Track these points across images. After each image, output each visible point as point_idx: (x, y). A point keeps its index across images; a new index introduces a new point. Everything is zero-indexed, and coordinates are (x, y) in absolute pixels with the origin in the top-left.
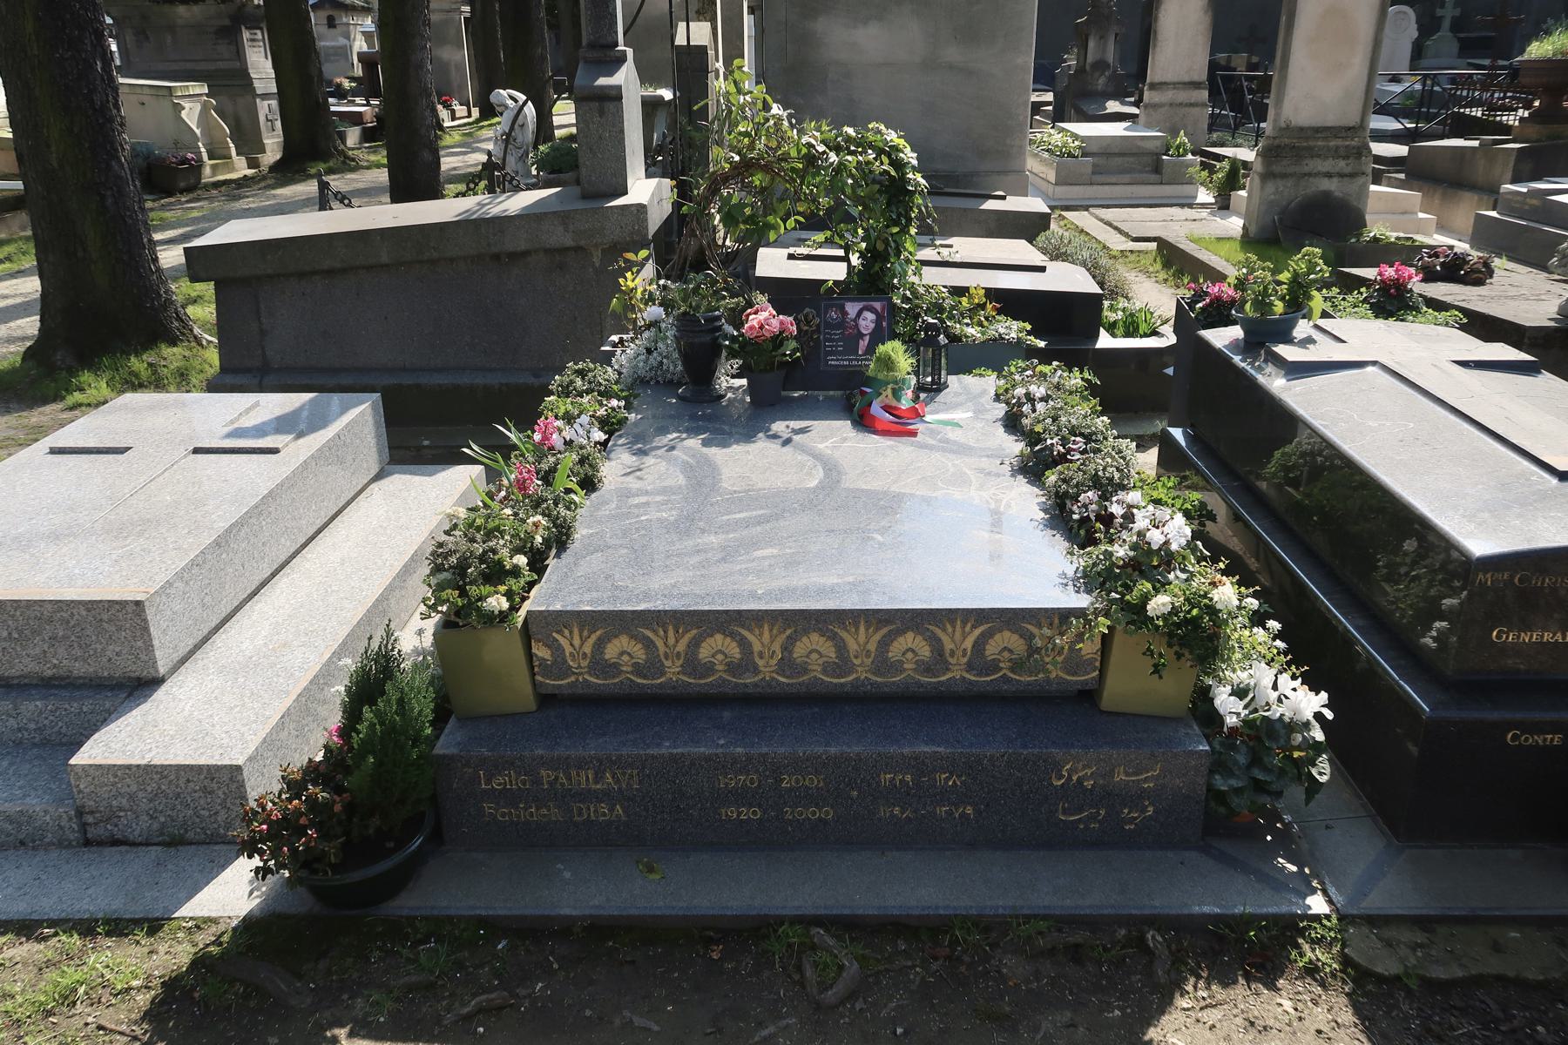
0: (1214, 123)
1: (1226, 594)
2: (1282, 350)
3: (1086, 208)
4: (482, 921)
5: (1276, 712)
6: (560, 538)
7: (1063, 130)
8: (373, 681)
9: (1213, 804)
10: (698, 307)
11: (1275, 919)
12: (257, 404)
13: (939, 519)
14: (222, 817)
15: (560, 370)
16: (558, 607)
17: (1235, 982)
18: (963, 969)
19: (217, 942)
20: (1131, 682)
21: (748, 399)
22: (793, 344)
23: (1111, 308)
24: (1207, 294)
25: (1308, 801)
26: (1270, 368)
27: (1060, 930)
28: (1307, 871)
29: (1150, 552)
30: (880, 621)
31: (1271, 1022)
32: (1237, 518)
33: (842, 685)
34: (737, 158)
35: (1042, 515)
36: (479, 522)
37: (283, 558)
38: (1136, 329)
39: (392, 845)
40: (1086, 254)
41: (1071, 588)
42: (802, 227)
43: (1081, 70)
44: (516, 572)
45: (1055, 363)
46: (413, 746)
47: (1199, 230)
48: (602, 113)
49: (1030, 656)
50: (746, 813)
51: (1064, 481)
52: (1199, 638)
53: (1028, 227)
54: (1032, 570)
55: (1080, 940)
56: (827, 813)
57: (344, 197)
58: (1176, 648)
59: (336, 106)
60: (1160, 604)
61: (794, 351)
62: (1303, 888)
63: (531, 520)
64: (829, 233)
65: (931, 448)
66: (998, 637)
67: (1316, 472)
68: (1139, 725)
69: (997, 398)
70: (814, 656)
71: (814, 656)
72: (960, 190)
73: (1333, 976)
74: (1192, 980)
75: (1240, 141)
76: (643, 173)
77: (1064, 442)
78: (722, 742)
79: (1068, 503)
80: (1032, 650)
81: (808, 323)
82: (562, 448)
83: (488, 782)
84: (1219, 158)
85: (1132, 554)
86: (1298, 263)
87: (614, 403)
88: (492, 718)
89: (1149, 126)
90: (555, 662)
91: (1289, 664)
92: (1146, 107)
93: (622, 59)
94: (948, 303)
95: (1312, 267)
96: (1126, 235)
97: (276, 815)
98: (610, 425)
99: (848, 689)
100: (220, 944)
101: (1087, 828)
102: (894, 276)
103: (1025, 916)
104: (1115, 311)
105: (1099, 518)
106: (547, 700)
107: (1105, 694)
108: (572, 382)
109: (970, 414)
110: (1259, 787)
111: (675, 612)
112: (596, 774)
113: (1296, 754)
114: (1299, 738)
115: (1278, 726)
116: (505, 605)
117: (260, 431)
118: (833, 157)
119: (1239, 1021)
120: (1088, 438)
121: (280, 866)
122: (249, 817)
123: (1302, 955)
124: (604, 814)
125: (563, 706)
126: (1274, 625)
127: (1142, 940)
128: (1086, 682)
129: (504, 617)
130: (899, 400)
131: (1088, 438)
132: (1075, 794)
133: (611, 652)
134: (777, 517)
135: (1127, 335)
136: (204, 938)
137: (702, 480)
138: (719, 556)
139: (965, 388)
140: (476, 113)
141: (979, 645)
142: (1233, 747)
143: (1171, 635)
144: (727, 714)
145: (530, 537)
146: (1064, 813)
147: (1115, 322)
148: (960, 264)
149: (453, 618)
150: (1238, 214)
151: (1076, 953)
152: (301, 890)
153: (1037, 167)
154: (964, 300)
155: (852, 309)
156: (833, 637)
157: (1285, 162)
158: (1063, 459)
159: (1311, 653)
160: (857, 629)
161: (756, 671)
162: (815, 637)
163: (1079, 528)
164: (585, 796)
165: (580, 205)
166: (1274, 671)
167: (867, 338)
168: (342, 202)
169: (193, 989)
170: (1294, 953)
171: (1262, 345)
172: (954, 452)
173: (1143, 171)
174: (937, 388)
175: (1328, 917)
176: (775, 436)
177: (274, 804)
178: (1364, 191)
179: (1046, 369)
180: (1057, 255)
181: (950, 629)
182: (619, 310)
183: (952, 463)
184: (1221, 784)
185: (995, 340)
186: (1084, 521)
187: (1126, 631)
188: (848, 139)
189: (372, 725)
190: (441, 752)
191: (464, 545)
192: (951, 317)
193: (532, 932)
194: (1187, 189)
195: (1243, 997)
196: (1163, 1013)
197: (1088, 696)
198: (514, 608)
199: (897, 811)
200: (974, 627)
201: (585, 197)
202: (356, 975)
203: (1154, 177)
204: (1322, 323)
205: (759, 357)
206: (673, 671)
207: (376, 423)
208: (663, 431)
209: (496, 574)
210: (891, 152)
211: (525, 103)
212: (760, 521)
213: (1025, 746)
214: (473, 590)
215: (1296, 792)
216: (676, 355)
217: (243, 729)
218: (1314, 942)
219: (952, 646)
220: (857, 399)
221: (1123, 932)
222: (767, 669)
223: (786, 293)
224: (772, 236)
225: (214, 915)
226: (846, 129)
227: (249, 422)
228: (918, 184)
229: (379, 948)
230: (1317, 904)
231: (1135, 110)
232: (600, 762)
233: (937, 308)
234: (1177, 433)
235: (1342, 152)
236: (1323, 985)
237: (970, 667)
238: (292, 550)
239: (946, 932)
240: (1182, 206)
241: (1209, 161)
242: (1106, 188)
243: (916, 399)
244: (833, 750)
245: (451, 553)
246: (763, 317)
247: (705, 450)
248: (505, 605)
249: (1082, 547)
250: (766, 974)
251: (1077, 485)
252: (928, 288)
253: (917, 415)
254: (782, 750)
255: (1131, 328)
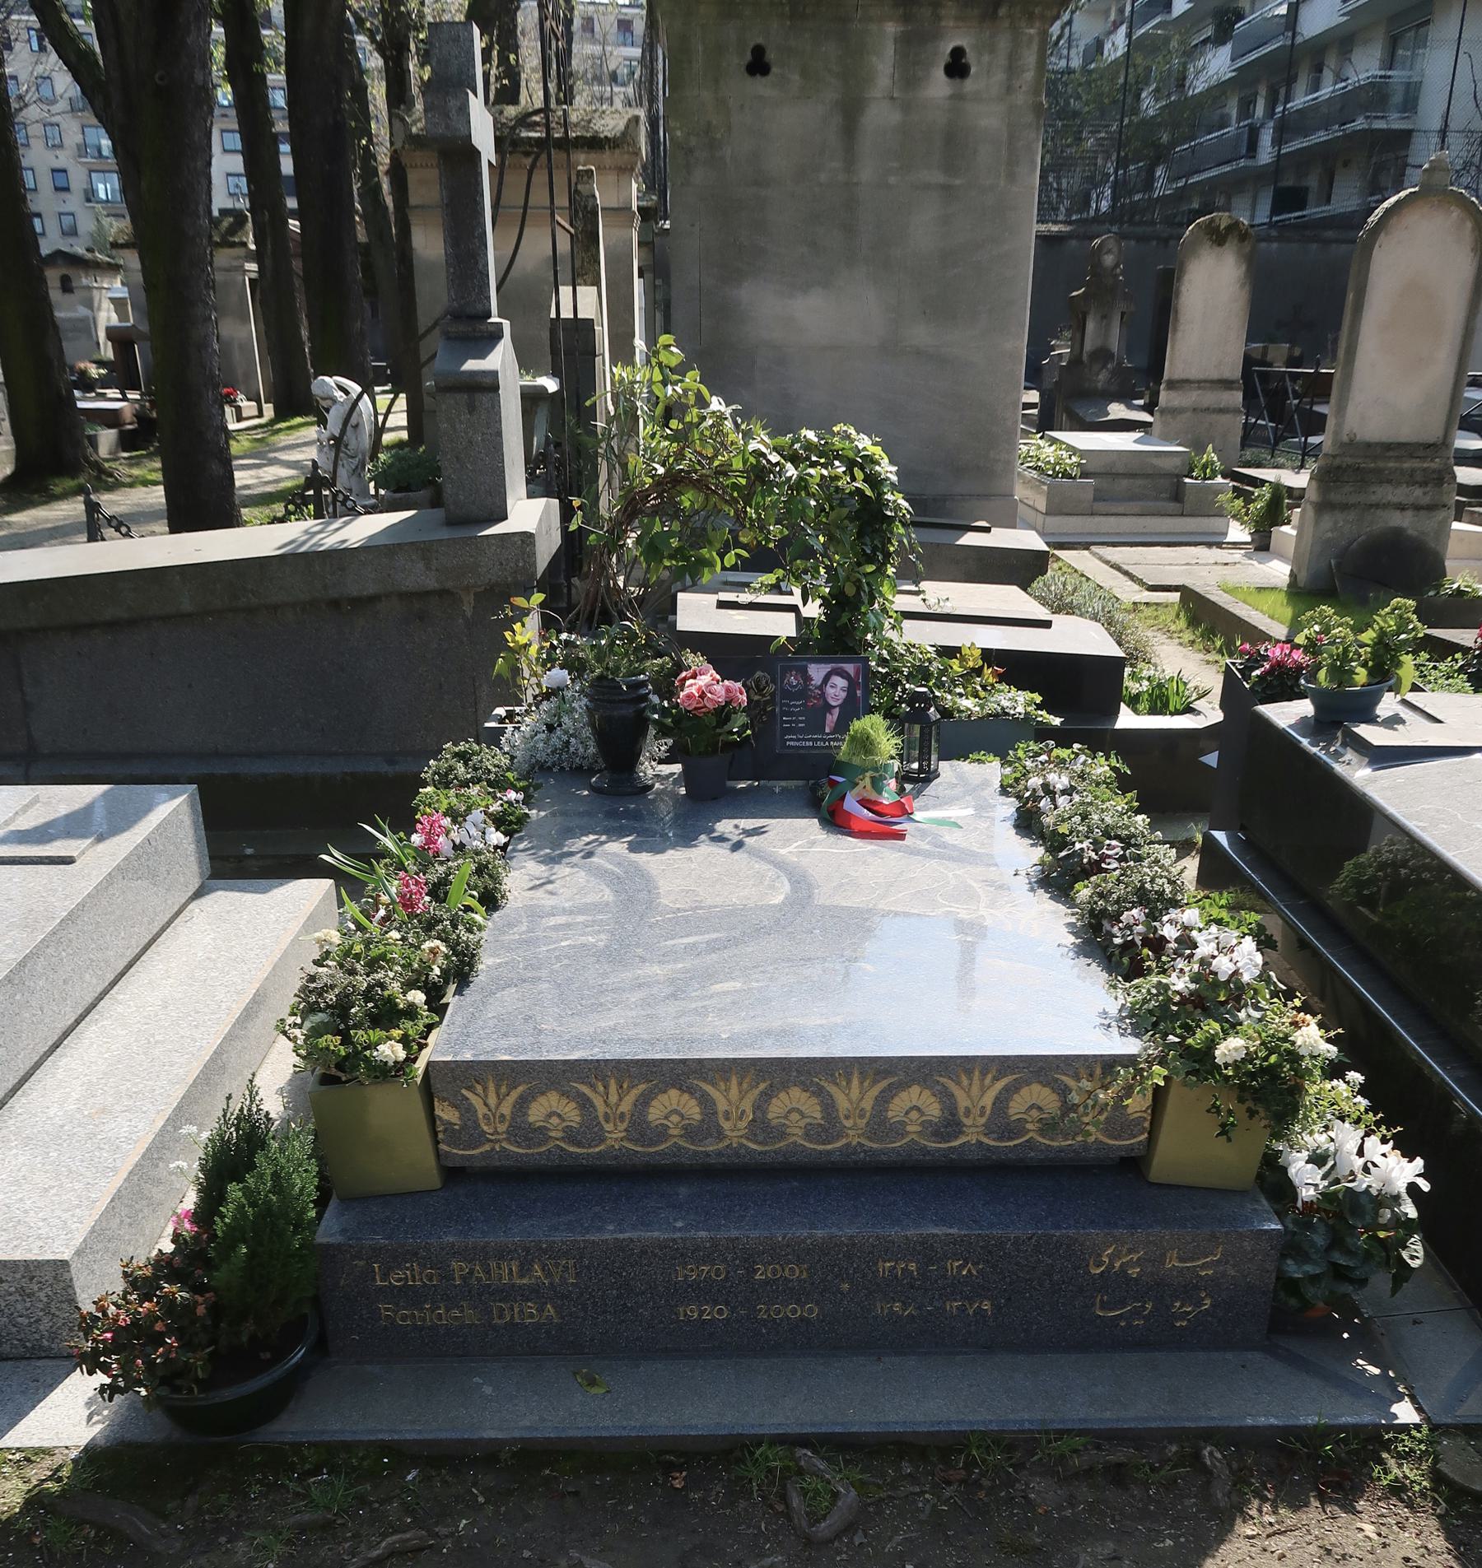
0: (1249, 436)
1: (1311, 1037)
2: (1363, 730)
3: (1086, 546)
4: (386, 1448)
5: (1363, 1183)
6: (462, 970)
7: (1054, 441)
8: (235, 1155)
9: (1282, 1294)
10: (618, 668)
11: (1355, 1430)
12: (36, 800)
13: (938, 947)
14: (45, 1325)
15: (436, 753)
16: (468, 1056)
17: (1307, 1504)
18: (982, 1495)
19: (55, 1476)
20: (1189, 1146)
21: (683, 791)
22: (742, 719)
23: (1133, 675)
24: (1265, 658)
25: (1394, 1291)
26: (1349, 755)
27: (1098, 1447)
28: (1391, 1374)
29: (1216, 985)
30: (878, 1073)
31: (1350, 1550)
32: (1303, 944)
33: (828, 1152)
34: (661, 470)
35: (1072, 939)
36: (358, 949)
37: (89, 1000)
38: (1166, 705)
39: (268, 1355)
40: (1097, 605)
41: (1115, 1031)
42: (747, 566)
43: (1076, 361)
44: (411, 1012)
45: (1076, 746)
46: (295, 1233)
47: (1234, 576)
48: (472, 408)
49: (1064, 1115)
50: (709, 1312)
51: (1101, 895)
52: (1274, 1091)
53: (1021, 569)
54: (1073, 1013)
55: (1123, 1459)
56: (811, 1310)
57: (121, 524)
58: (1250, 1104)
59: (86, 403)
60: (1230, 1049)
61: (744, 727)
62: (1388, 1394)
63: (427, 945)
64: (780, 572)
65: (928, 855)
66: (1024, 1091)
67: (1398, 889)
68: (1198, 1199)
69: (1004, 791)
70: (795, 1116)
71: (795, 1116)
72: (934, 516)
73: (1423, 1495)
74: (1256, 1503)
75: (1281, 460)
76: (522, 490)
77: (1097, 845)
78: (679, 1224)
79: (1106, 925)
80: (1067, 1108)
81: (760, 690)
82: (451, 854)
83: (385, 1277)
84: (1258, 483)
85: (1193, 986)
86: (1386, 620)
87: (512, 795)
88: (386, 1198)
89: (1166, 438)
90: (464, 1127)
91: (1378, 1124)
92: (1162, 412)
93: (496, 335)
94: (936, 666)
95: (1402, 626)
96: (1140, 582)
97: (124, 1319)
98: (506, 822)
99: (835, 1158)
100: (60, 1480)
101: (1129, 1325)
102: (866, 630)
103: (1057, 1431)
104: (1139, 680)
105: (1146, 942)
106: (453, 1174)
107: (1156, 1161)
108: (451, 769)
109: (971, 811)
110: (1340, 1274)
111: (619, 1061)
112: (522, 1265)
113: (1382, 1234)
114: (1388, 1214)
115: (1364, 1200)
116: (402, 1055)
117: (42, 834)
118: (791, 471)
119: (1313, 1549)
120: (1127, 842)
121: (132, 1383)
122: (87, 1324)
123: (1386, 1472)
124: (531, 1316)
125: (480, 1182)
126: (1355, 1077)
127: (1197, 1456)
128: (1131, 1148)
129: (402, 1068)
130: (880, 792)
131: (1127, 842)
132: (1117, 1285)
133: (536, 1113)
134: (736, 942)
135: (1153, 711)
136: (37, 1472)
137: (635, 896)
138: (668, 991)
139: (961, 777)
140: (269, 410)
141: (1001, 1102)
142: (1309, 1226)
143: (1242, 1087)
144: (683, 1191)
145: (426, 967)
146: (1102, 1308)
147: (1138, 695)
148: (938, 617)
149: (334, 1071)
150: (1281, 557)
151: (1118, 1475)
152: (158, 1415)
153: (1028, 494)
154: (955, 664)
155: (817, 672)
156: (819, 1092)
157: (1347, 489)
158: (1096, 868)
159: (1402, 1109)
160: (849, 1082)
161: (720, 1135)
162: (796, 1092)
163: (1122, 955)
164: (508, 1293)
165: (445, 534)
166: (1361, 1133)
167: (836, 712)
168: (118, 530)
169: (32, 1533)
170: (1377, 1469)
171: (1338, 724)
172: (951, 858)
173: (1157, 498)
174: (926, 777)
175: (1417, 1427)
176: (721, 839)
177: (118, 1307)
178: (1443, 531)
179: (1064, 753)
180: (1062, 606)
181: (965, 1082)
182: (507, 674)
183: (954, 873)
184: (1294, 1270)
185: (996, 715)
186: (1128, 946)
187: (1185, 1084)
188: (809, 446)
189: (241, 1207)
190: (324, 1240)
191: (342, 978)
192: (940, 685)
193: (447, 1459)
194: (1214, 523)
195: (1316, 1521)
196: (1222, 1541)
197: (1133, 1165)
198: (411, 1059)
199: (897, 1307)
200: (996, 1079)
201: (452, 522)
202: (233, 1514)
203: (1172, 506)
204: (1412, 697)
205: (695, 735)
206: (615, 1135)
207: (195, 823)
208: (570, 833)
209: (387, 1015)
210: (858, 463)
211: (360, 396)
212: (712, 947)
213: (1058, 1227)
214: (360, 1036)
215: (1381, 1281)
216: (587, 732)
217: (65, 1216)
218: (1400, 1457)
219: (968, 1103)
220: (821, 789)
221: (1174, 1448)
222: (735, 1132)
223: (728, 652)
224: (706, 577)
225: (46, 1444)
226: (804, 432)
227: (25, 823)
228: (898, 508)
229: (258, 1481)
230: (1405, 1412)
231: (1145, 417)
232: (527, 1250)
233: (922, 673)
234: (1221, 836)
235: (1419, 477)
236: (1410, 1505)
237: (988, 1130)
238: (99, 989)
239: (960, 1452)
240: (1209, 545)
241: (1245, 486)
242: (1112, 519)
243: (901, 791)
244: (819, 1233)
245: (327, 988)
246: (703, 682)
247: (633, 856)
248: (402, 1055)
249: (1127, 979)
250: (742, 1504)
251: (1117, 902)
252: (909, 647)
253: (904, 812)
254: (755, 1234)
255: (1159, 703)
